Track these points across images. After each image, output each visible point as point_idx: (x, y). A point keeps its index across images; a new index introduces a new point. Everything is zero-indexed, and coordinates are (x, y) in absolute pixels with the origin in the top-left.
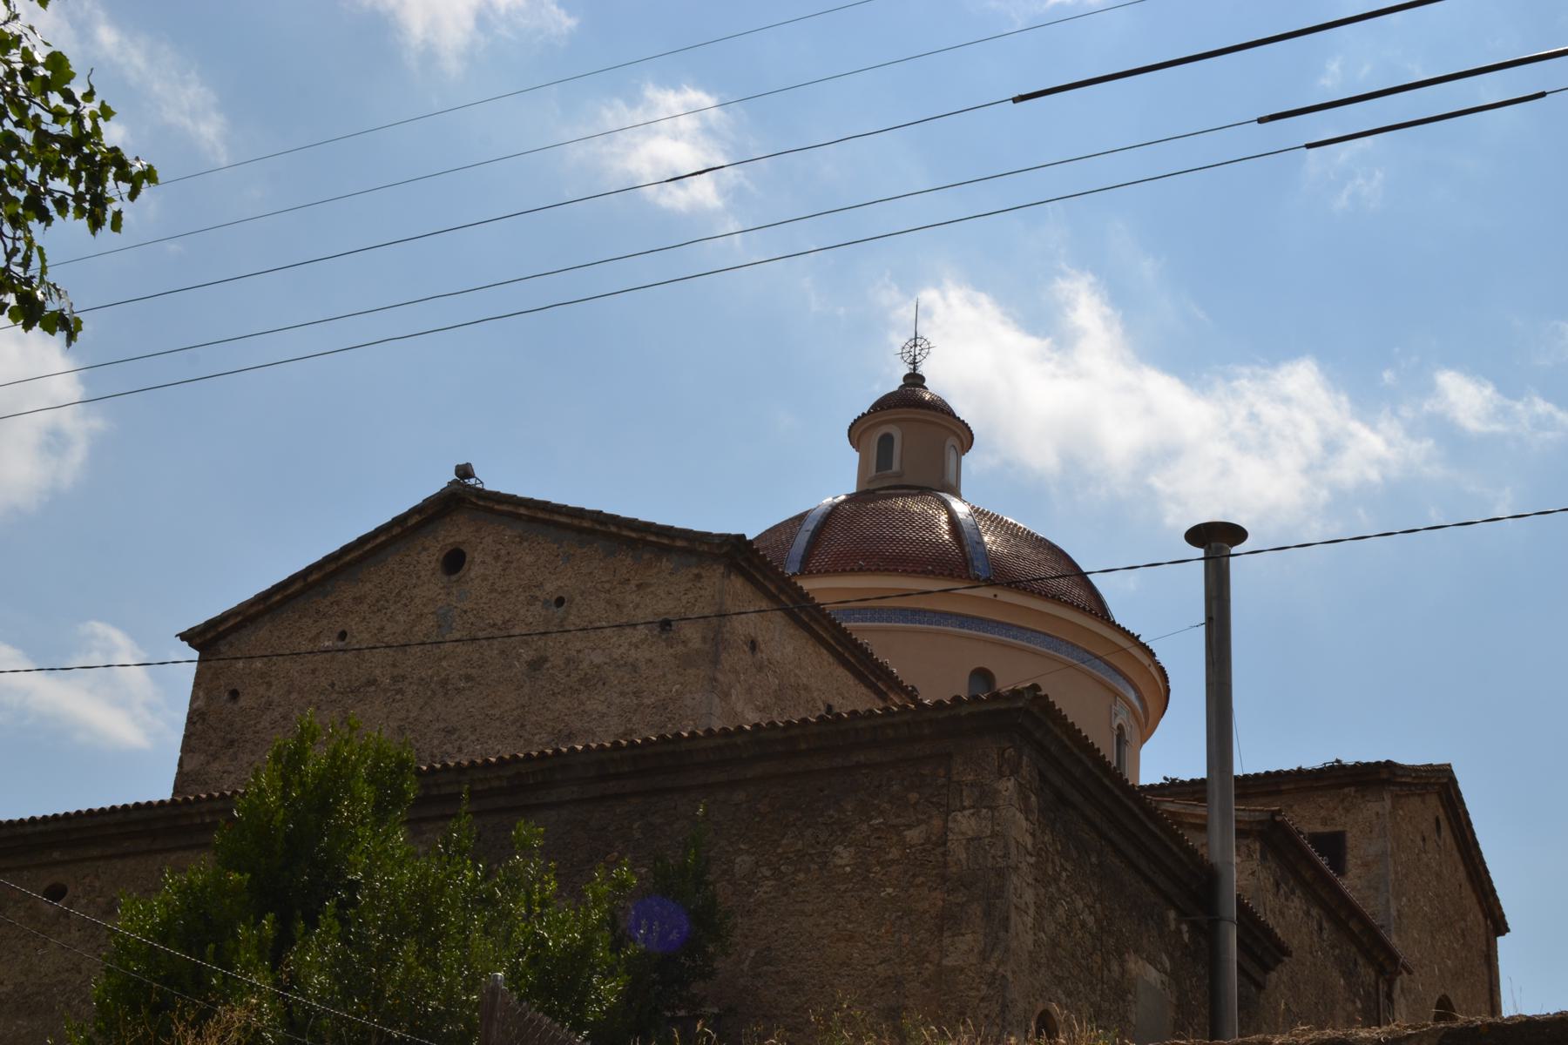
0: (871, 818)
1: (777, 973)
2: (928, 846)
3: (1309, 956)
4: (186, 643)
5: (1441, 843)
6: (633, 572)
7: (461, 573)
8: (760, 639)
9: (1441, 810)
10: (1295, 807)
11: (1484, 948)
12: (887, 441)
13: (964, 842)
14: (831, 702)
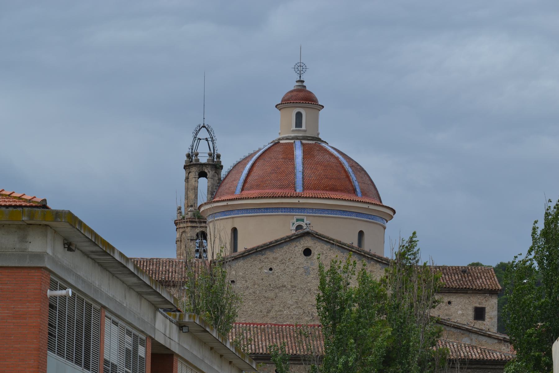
7: (311, 256)
10: (471, 298)
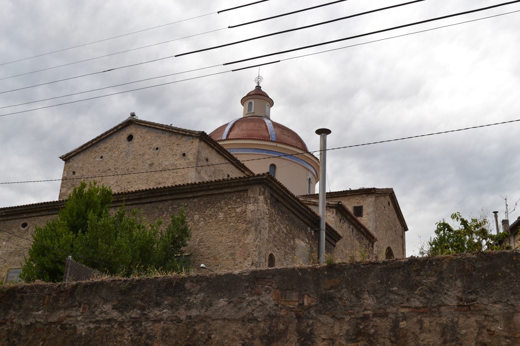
0: (228, 206)
1: (204, 244)
2: (242, 213)
3: (349, 238)
4: (61, 159)
5: (390, 208)
6: (176, 141)
7: (132, 141)
8: (209, 158)
9: (390, 200)
11: (401, 234)
12: (250, 103)
13: (250, 212)
14: (229, 174)
